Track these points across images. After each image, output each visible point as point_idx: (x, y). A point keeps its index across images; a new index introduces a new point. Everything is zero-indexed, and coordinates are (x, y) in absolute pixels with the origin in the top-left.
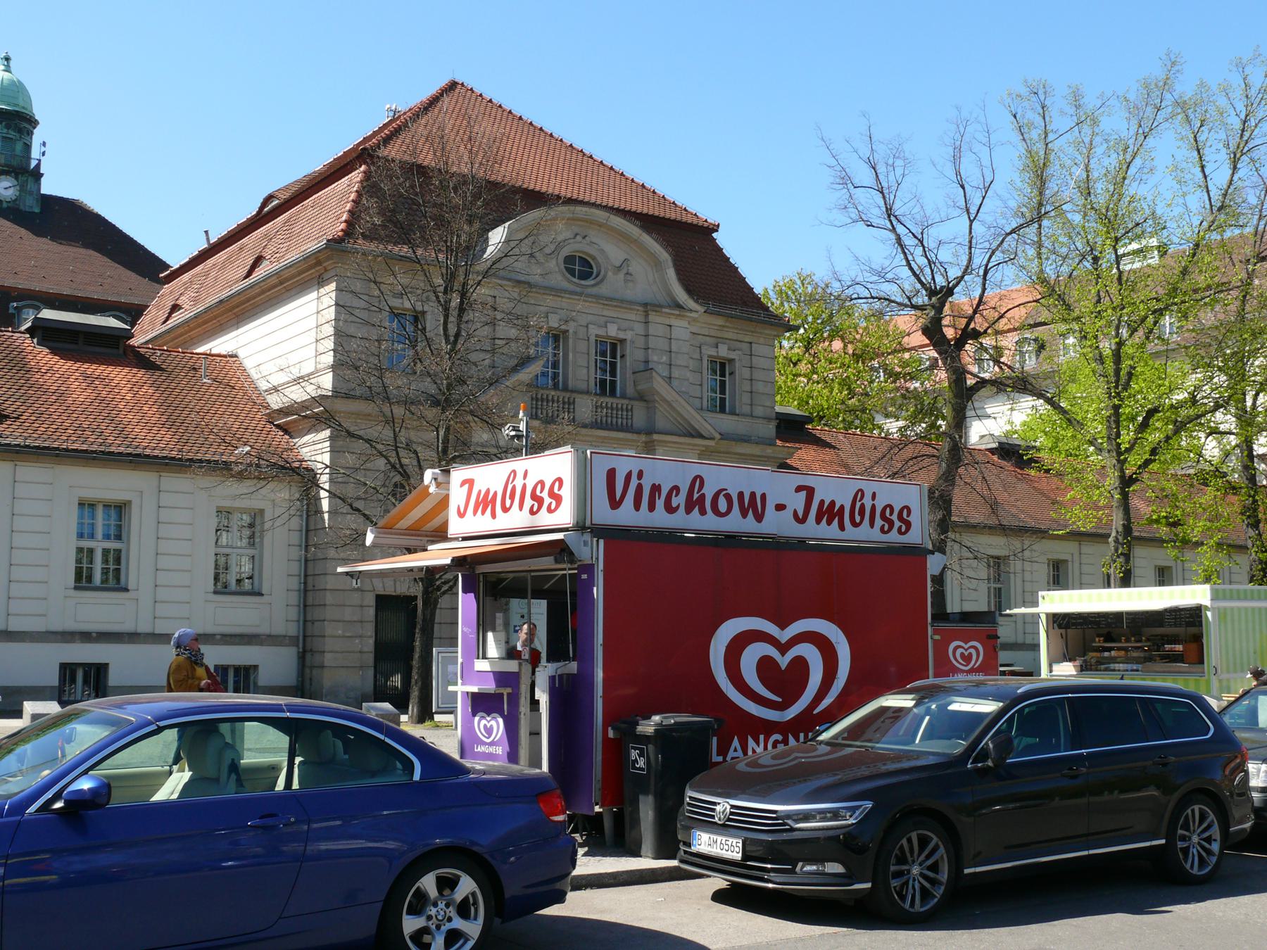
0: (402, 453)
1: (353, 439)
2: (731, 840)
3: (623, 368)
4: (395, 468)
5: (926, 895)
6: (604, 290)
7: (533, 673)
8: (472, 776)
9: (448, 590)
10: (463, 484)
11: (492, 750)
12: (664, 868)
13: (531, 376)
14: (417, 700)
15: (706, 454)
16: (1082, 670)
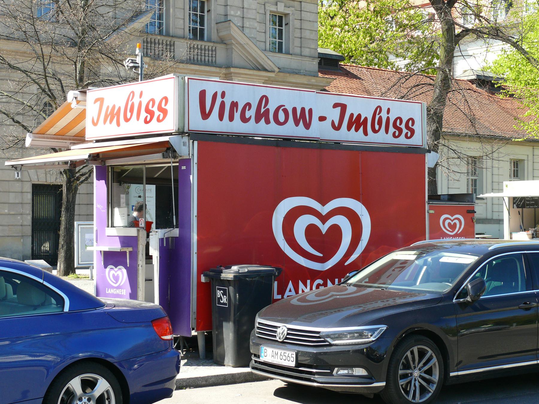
0: (50, 81)
1: (13, 70)
2: (288, 352)
3: (209, 19)
4: (45, 92)
5: (423, 390)
7: (148, 236)
8: (106, 308)
9: (84, 180)
10: (96, 101)
11: (118, 292)
12: (241, 373)
13: (143, 25)
14: (63, 260)
15: (268, 82)
16: (533, 237)
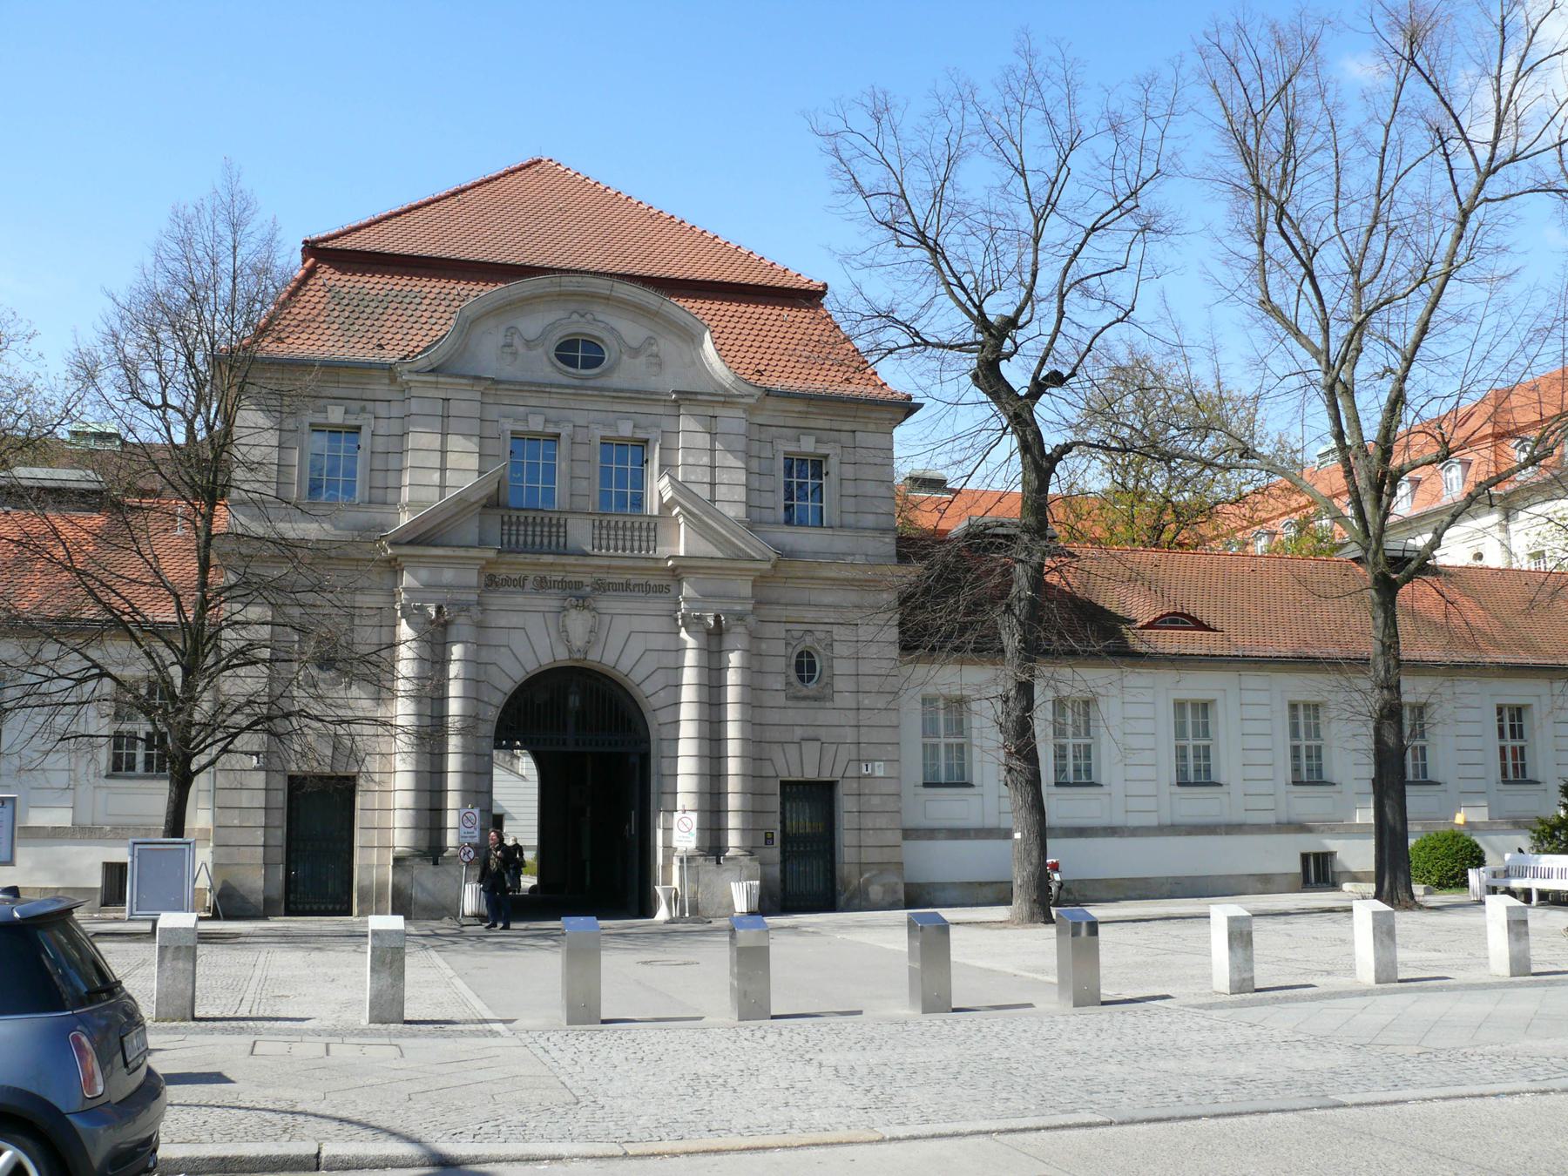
6: (618, 380)
